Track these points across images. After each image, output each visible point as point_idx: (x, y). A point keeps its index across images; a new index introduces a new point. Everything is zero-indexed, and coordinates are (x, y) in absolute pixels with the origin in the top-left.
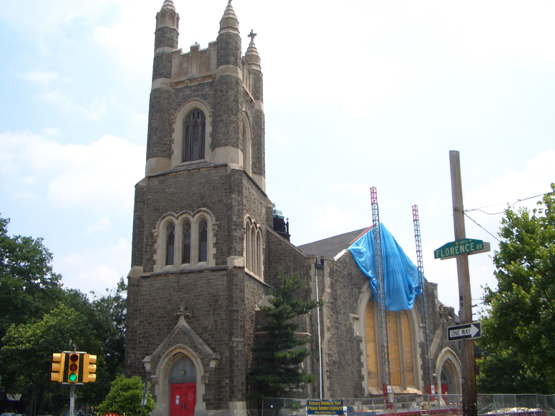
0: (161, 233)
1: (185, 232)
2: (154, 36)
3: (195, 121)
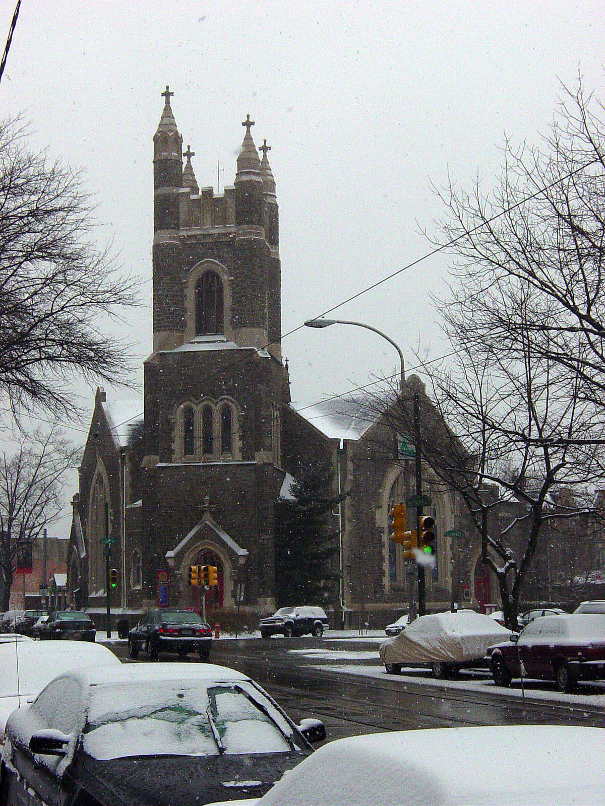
0: (178, 419)
1: (206, 419)
2: (152, 166)
3: (209, 287)
